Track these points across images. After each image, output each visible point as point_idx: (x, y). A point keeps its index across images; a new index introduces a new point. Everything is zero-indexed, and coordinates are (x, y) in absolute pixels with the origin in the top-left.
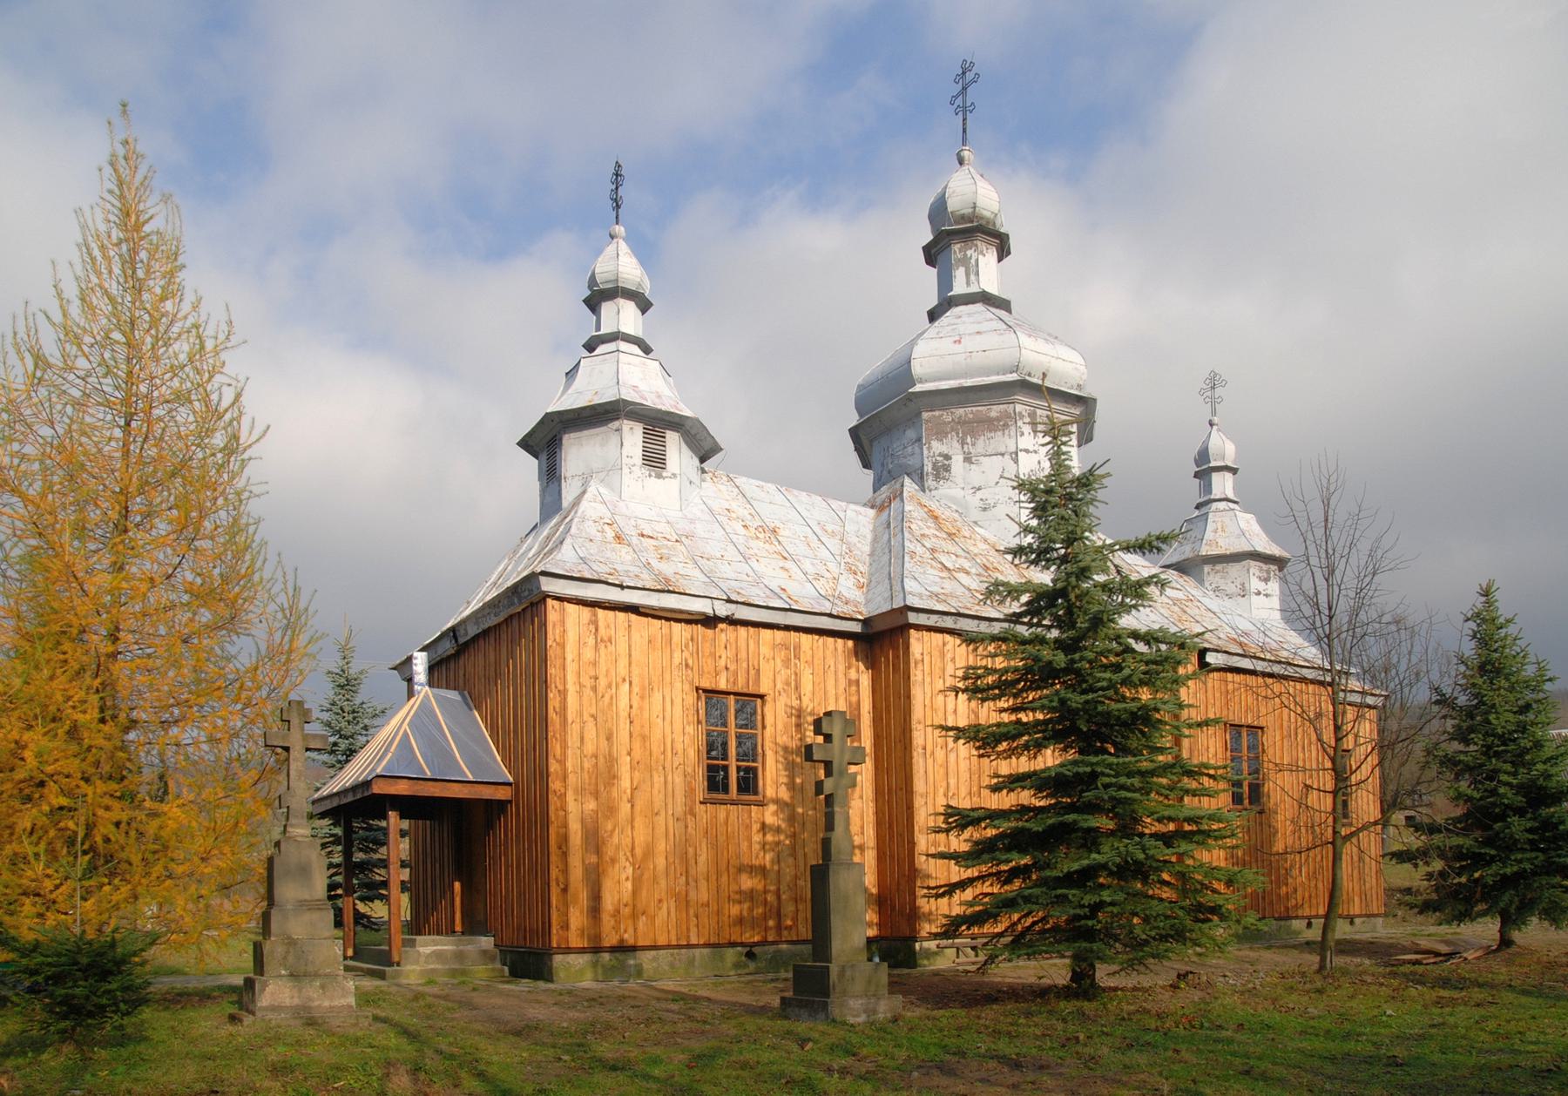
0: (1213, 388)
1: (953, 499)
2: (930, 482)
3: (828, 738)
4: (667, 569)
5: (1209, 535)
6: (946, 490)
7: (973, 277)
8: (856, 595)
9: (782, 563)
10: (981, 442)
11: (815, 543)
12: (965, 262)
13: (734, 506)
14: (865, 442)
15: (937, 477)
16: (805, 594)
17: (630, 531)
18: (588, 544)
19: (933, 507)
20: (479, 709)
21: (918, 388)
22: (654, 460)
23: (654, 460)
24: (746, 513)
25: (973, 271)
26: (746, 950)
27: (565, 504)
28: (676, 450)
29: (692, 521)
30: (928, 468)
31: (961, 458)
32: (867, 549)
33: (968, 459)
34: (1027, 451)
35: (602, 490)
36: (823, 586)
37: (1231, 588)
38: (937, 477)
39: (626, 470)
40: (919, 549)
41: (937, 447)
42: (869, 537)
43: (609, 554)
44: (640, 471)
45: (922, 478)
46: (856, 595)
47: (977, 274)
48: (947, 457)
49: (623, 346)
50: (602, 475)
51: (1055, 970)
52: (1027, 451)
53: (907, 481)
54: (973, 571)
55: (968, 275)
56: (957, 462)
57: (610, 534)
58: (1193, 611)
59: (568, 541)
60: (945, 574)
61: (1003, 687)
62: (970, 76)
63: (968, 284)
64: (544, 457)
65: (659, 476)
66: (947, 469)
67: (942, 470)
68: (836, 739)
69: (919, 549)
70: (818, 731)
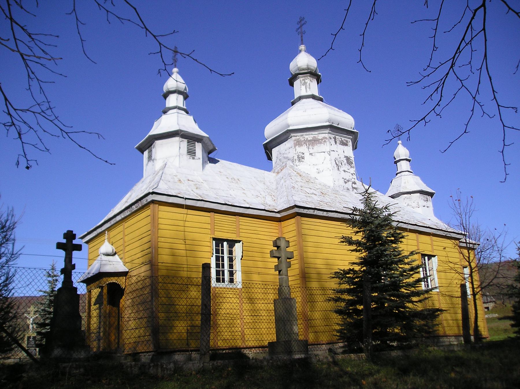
7: (308, 89)
23: (191, 153)
47: (310, 88)
55: (306, 89)
57: (176, 180)
62: (302, 22)
65: (193, 158)
66: (303, 158)
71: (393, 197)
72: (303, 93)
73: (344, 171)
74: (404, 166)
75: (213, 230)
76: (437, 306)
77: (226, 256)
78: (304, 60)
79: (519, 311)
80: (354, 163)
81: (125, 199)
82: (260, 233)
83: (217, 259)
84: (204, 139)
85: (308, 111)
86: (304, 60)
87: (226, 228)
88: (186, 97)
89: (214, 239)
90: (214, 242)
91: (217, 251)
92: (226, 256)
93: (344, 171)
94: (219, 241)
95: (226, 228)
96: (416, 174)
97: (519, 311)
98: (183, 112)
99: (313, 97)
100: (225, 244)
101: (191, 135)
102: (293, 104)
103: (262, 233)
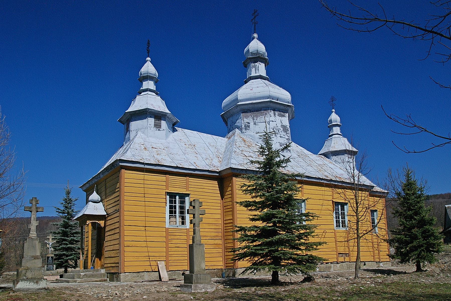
0: (332, 101)
1: (251, 136)
2: (244, 131)
3: (194, 207)
4: (159, 157)
5: (332, 145)
6: (248, 132)
7: (257, 71)
8: (218, 164)
9: (196, 155)
10: (259, 118)
11: (207, 149)
12: (255, 67)
13: (182, 138)
14: (226, 119)
15: (246, 129)
16: (202, 165)
17: (149, 146)
18: (135, 151)
19: (244, 138)
20: (265, 200)
21: (239, 103)
22: (158, 126)
23: (158, 126)
24: (186, 140)
25: (257, 69)
26: (182, 272)
27: (131, 139)
28: (164, 124)
29: (169, 143)
30: (243, 126)
31: (253, 123)
32: (223, 150)
33: (255, 124)
34: (273, 121)
35: (142, 135)
36: (208, 162)
37: (340, 161)
38: (246, 129)
39: (149, 128)
40: (238, 151)
41: (246, 120)
42: (225, 147)
43: (141, 153)
44: (153, 129)
45: (241, 129)
46: (218, 164)
47: (258, 70)
48: (249, 123)
49: (149, 93)
50: (142, 130)
51: (265, 275)
52: (273, 121)
53: (237, 130)
54: (254, 157)
55: (256, 70)
56: (252, 124)
57: (143, 147)
58: (325, 168)
59: (130, 150)
60: (245, 158)
61: (251, 191)
62: (256, 14)
63: (256, 73)
64: (126, 125)
65: (159, 130)
66: (249, 127)
67: (247, 127)
68: (196, 207)
69: (238, 151)
70: (191, 205)
71: (326, 155)
72: (253, 74)
73: (281, 137)
74: (337, 130)
75: (167, 186)
76: (386, 244)
77: (178, 205)
78: (256, 45)
79: (1, 230)
80: (289, 130)
81: (110, 161)
82: (205, 187)
83: (171, 207)
84: (168, 115)
85: (257, 88)
86: (256, 45)
87: (178, 185)
88: (156, 83)
89: (168, 193)
90: (168, 197)
91: (171, 202)
92: (178, 205)
93: (281, 137)
94: (172, 196)
95: (178, 185)
96: (344, 136)
97: (1, 230)
98: (154, 94)
99: (261, 77)
100: (177, 197)
101: (157, 112)
102: (246, 82)
103: (205, 187)
